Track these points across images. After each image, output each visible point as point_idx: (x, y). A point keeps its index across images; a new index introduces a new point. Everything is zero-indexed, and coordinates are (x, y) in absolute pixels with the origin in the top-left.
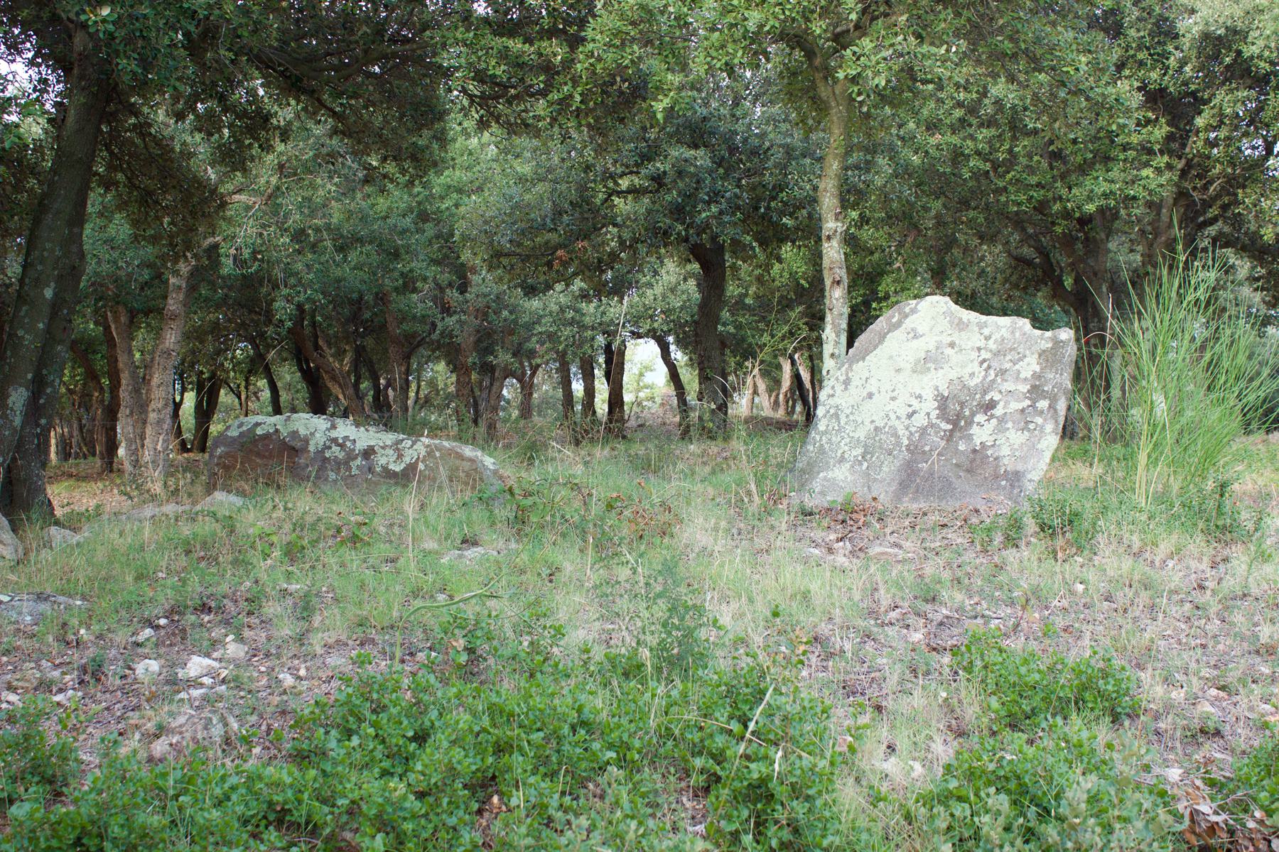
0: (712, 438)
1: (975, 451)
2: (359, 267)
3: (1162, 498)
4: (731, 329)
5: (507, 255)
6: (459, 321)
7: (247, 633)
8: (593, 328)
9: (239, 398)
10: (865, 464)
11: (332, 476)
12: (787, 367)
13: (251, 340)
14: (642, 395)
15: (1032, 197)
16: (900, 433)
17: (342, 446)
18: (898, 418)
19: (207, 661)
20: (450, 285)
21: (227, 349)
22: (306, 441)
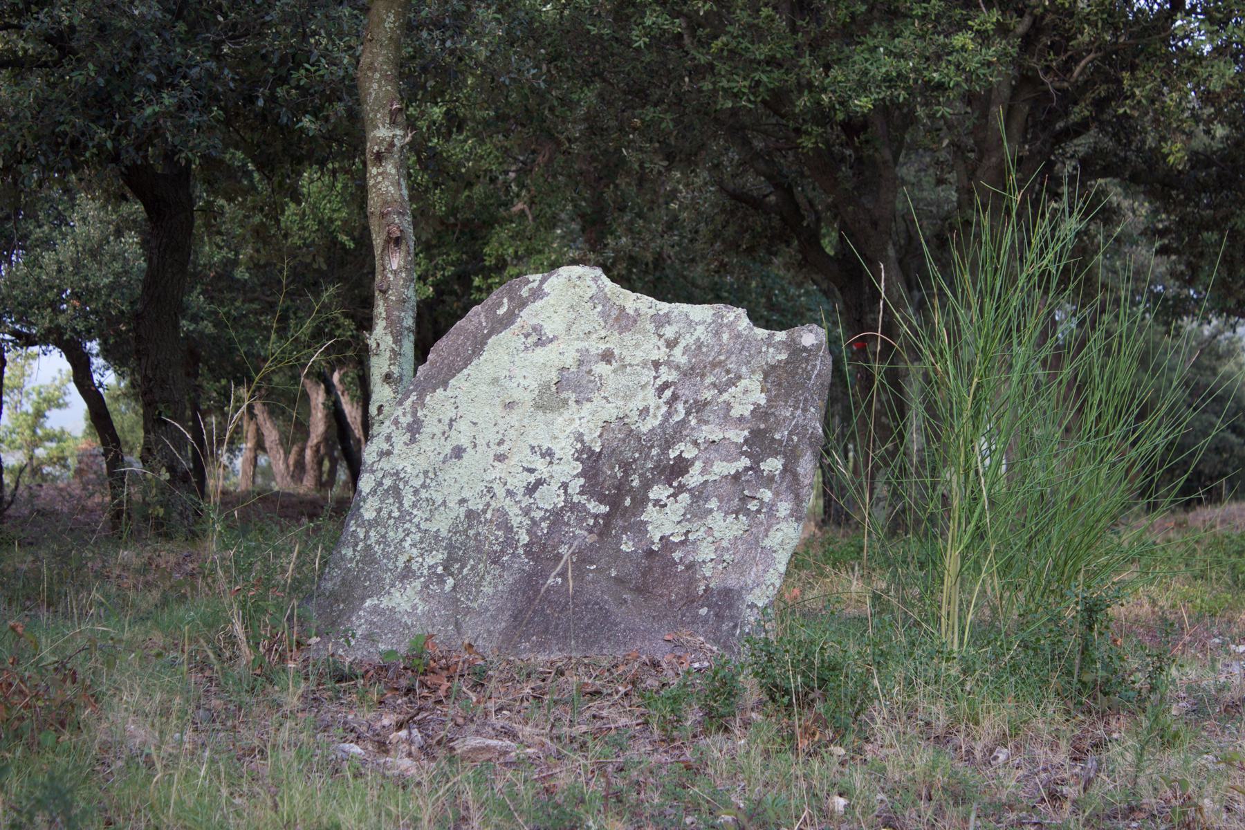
0: (168, 536)
1: (650, 553)
3: (984, 633)
4: (208, 327)
10: (450, 582)
12: (318, 397)
14: (40, 452)
15: (758, 83)
16: (515, 522)
18: (510, 493)
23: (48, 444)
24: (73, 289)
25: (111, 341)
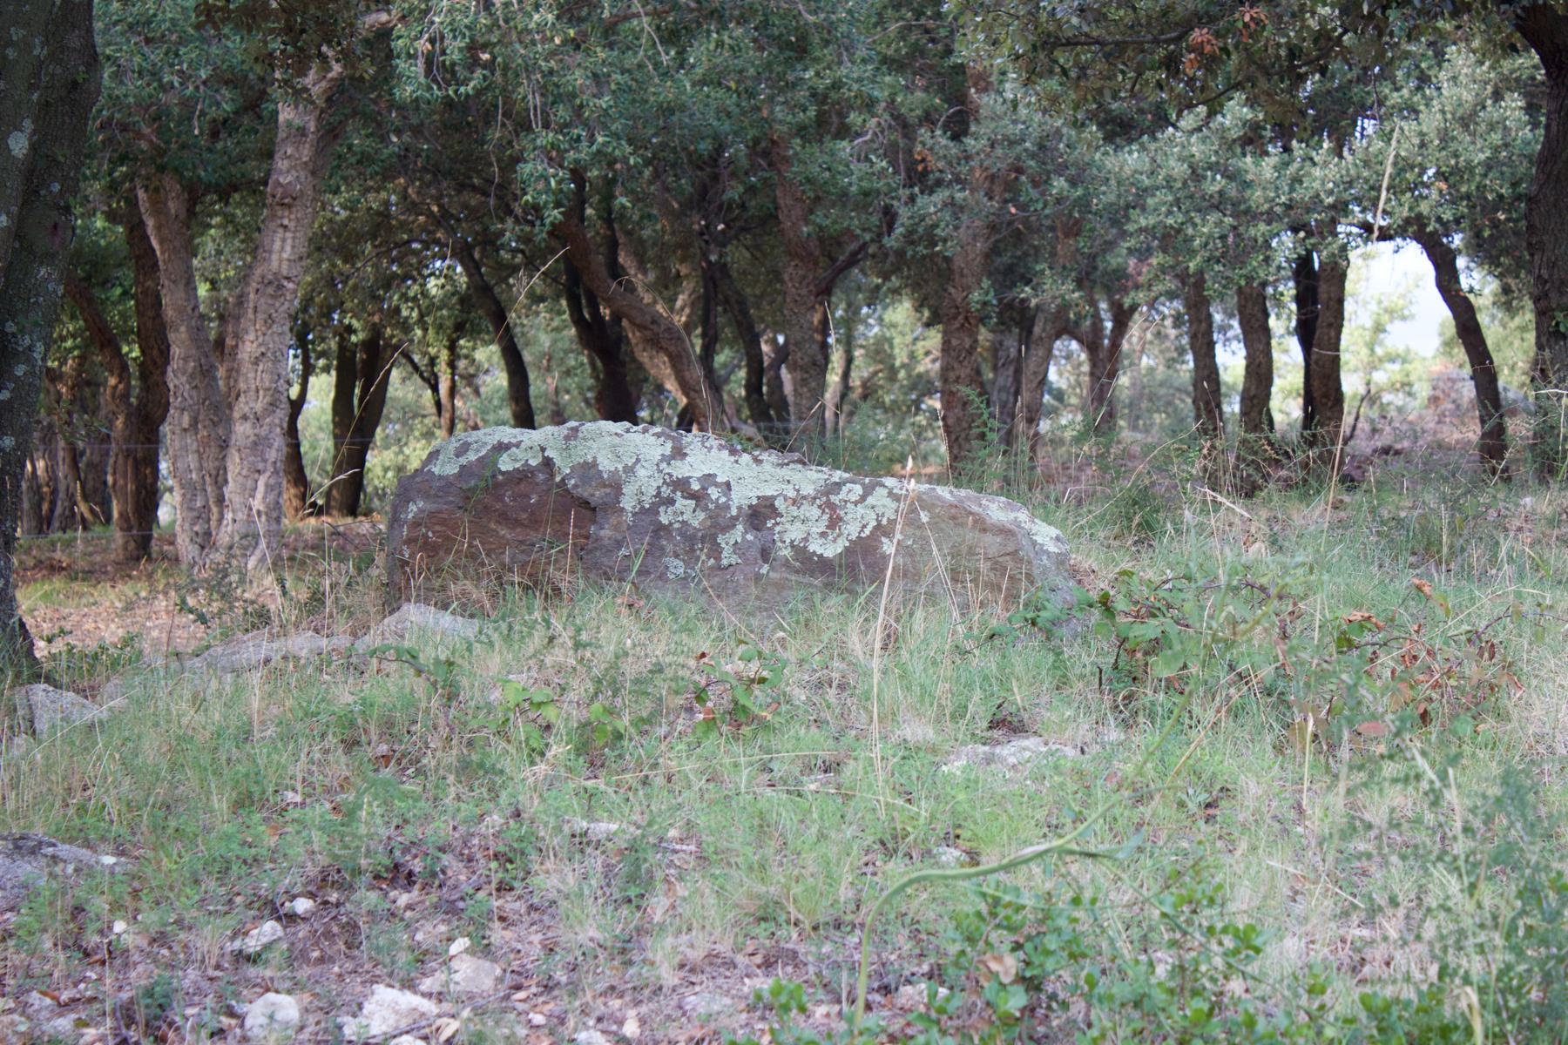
2: (714, 79)
5: (1071, 43)
6: (951, 203)
7: (498, 935)
8: (1270, 217)
9: (435, 388)
11: (677, 567)
13: (463, 253)
14: (1380, 377)
17: (699, 497)
19: (409, 1000)
20: (928, 119)
21: (407, 277)
22: (617, 488)
23: (1389, 366)
24: (1439, 168)
25: (1486, 233)
